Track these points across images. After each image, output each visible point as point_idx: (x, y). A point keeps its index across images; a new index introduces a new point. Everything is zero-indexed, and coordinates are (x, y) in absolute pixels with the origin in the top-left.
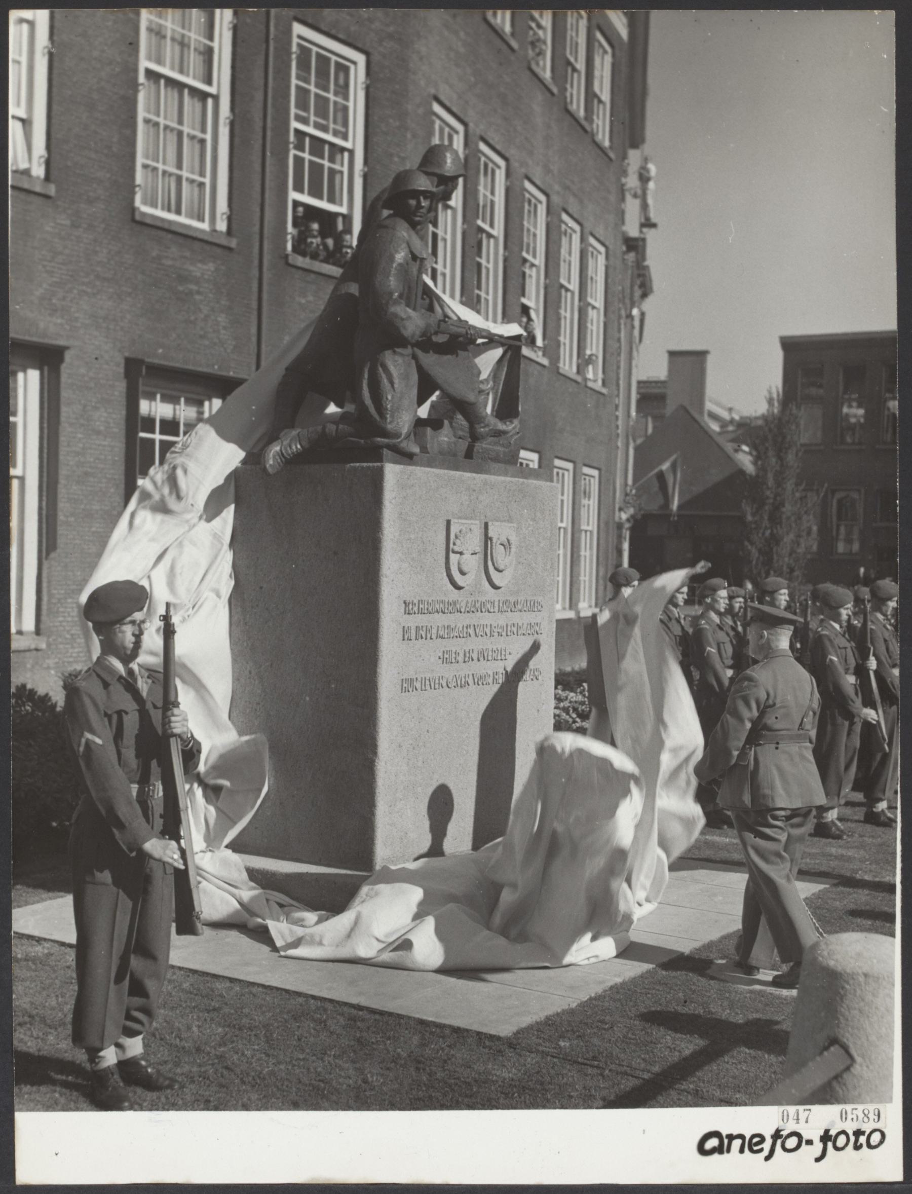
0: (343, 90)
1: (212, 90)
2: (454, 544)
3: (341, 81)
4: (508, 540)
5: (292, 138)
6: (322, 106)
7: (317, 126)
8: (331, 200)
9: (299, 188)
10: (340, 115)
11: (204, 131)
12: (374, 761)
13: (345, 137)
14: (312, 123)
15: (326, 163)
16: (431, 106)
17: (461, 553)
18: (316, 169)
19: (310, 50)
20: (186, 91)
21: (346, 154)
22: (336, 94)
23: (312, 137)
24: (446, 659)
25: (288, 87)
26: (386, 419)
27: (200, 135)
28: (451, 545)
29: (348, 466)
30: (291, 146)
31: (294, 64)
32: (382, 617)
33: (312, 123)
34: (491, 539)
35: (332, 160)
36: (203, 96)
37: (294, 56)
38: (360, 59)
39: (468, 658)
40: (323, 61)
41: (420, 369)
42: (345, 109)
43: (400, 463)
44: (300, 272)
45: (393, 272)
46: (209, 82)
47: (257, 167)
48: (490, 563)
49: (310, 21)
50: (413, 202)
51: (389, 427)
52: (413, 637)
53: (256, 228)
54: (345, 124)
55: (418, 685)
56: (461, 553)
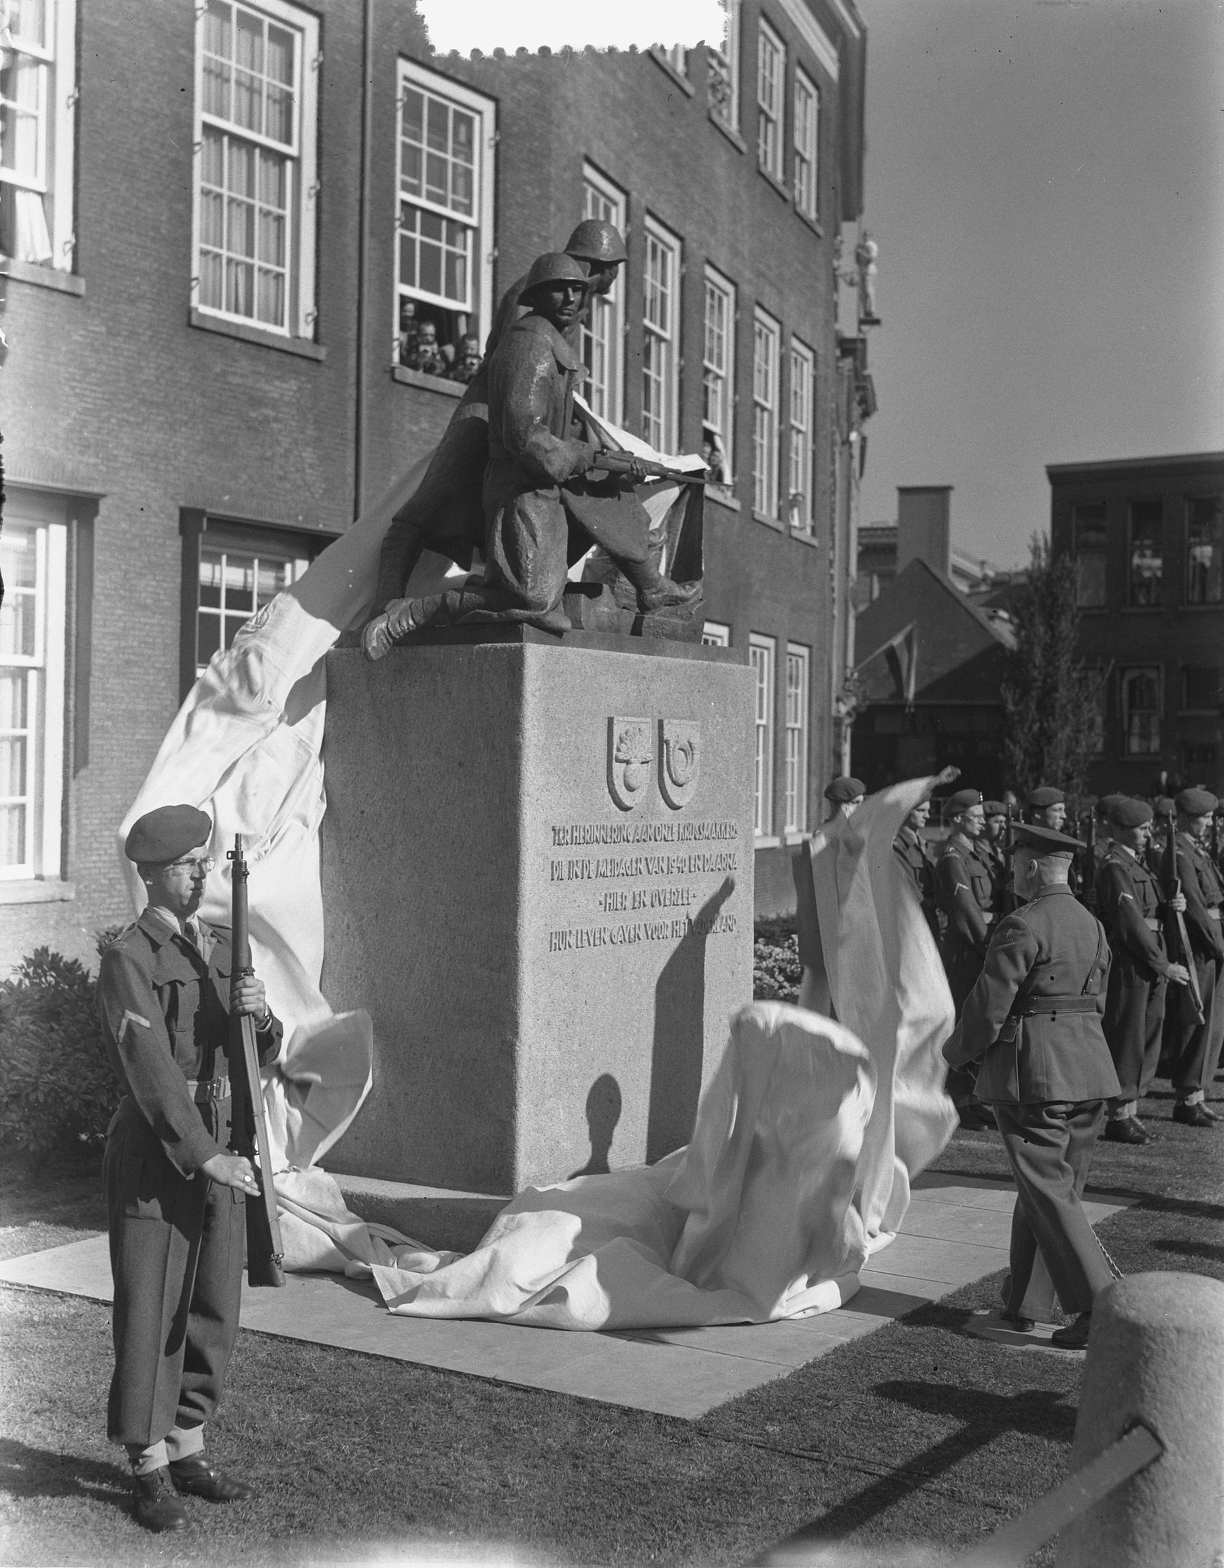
0: (465, 148)
1: (292, 151)
2: (618, 750)
4: (690, 744)
7: (431, 197)
8: (451, 294)
10: (461, 182)
11: (281, 205)
13: (469, 212)
14: (424, 193)
15: (444, 246)
16: (581, 169)
17: (628, 762)
18: (431, 254)
19: (421, 96)
21: (470, 233)
22: (455, 154)
23: (425, 211)
26: (527, 583)
28: (615, 752)
30: (397, 223)
33: (424, 193)
34: (667, 742)
35: (451, 241)
36: (282, 158)
37: (399, 104)
38: (487, 107)
39: (638, 904)
40: (438, 110)
42: (468, 173)
44: (411, 390)
45: (534, 388)
46: (288, 141)
47: (353, 251)
48: (666, 775)
50: (559, 296)
52: (565, 876)
53: (352, 334)
54: (469, 193)
55: (573, 941)
56: (628, 762)
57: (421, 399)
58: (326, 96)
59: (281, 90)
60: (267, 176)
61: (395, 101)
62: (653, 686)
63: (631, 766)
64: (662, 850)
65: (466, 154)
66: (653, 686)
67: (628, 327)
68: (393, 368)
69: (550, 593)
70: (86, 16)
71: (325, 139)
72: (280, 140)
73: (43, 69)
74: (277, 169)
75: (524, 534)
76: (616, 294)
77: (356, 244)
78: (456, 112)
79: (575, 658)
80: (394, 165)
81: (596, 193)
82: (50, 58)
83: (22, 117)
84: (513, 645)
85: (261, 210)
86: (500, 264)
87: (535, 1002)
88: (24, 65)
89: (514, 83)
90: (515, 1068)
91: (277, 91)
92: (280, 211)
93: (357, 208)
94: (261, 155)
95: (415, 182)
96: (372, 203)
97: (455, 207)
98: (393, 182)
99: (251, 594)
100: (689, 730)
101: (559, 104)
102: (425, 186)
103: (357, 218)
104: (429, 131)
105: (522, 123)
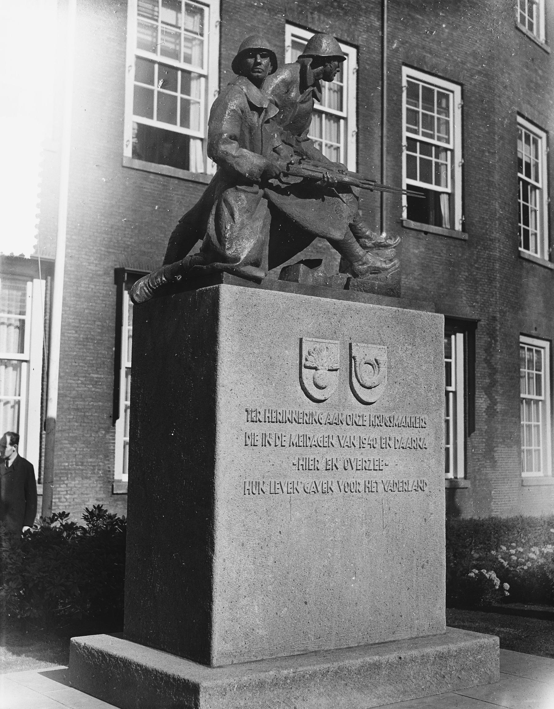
0: (446, 111)
1: (343, 114)
2: (306, 360)
3: (444, 105)
4: (376, 360)
5: (404, 142)
6: (428, 122)
7: (424, 134)
8: (438, 183)
9: (411, 175)
10: (443, 128)
11: (338, 141)
12: (212, 558)
13: (448, 141)
14: (421, 133)
15: (434, 159)
16: (516, 119)
17: (316, 369)
18: (426, 164)
19: (418, 85)
20: (324, 116)
21: (449, 153)
22: (439, 113)
23: (421, 142)
24: (306, 466)
25: (400, 110)
26: (225, 245)
27: (335, 144)
28: (304, 361)
29: (197, 290)
30: (404, 148)
31: (404, 95)
32: (219, 422)
33: (421, 133)
34: (354, 358)
35: (437, 157)
36: (337, 119)
37: (404, 89)
38: (457, 89)
39: (331, 467)
40: (428, 93)
41: (272, 206)
42: (447, 123)
43: (240, 285)
44: (413, 232)
45: (227, 117)
46: (341, 110)
47: (377, 162)
48: (354, 380)
49: (415, 65)
50: (251, 61)
51: (229, 252)
52: (259, 443)
53: (378, 204)
54: (448, 133)
55: (266, 488)
56: (316, 369)
57: (420, 236)
58: (360, 86)
59: (338, 85)
60: (330, 129)
61: (402, 87)
62: (343, 320)
63: (318, 371)
64: (353, 432)
65: (446, 113)
66: (343, 320)
67: (549, 200)
68: (402, 221)
69: (242, 251)
70: (224, 53)
71: (360, 107)
72: (338, 110)
73: (203, 79)
74: (336, 124)
75: (226, 213)
76: (542, 183)
77: (379, 159)
78: (438, 92)
79: (272, 299)
80: (401, 119)
81: (527, 132)
82: (205, 74)
83: (193, 103)
84: (214, 286)
85: (326, 145)
86: (465, 167)
87: (229, 529)
88: (194, 78)
89: (472, 76)
90: (212, 575)
91: (336, 86)
92: (338, 145)
93: (380, 140)
94: (326, 118)
95: (416, 128)
96: (388, 138)
97: (439, 139)
98: (401, 128)
99: (38, 261)
100: (376, 351)
101: (500, 86)
102: (421, 129)
103: (380, 146)
104: (422, 102)
105: (477, 96)
